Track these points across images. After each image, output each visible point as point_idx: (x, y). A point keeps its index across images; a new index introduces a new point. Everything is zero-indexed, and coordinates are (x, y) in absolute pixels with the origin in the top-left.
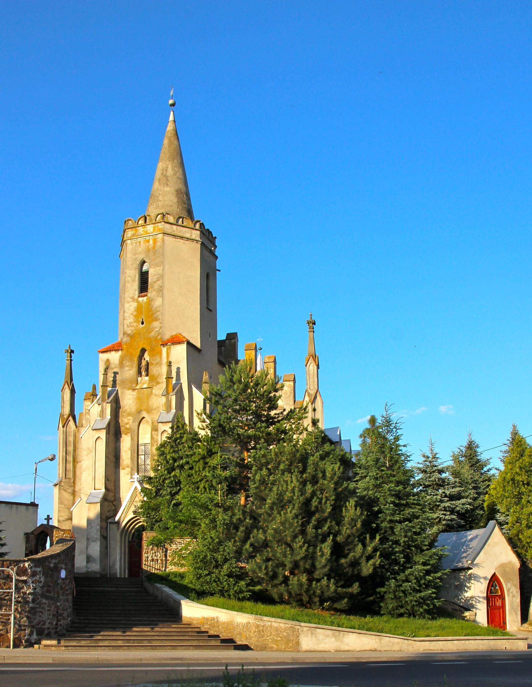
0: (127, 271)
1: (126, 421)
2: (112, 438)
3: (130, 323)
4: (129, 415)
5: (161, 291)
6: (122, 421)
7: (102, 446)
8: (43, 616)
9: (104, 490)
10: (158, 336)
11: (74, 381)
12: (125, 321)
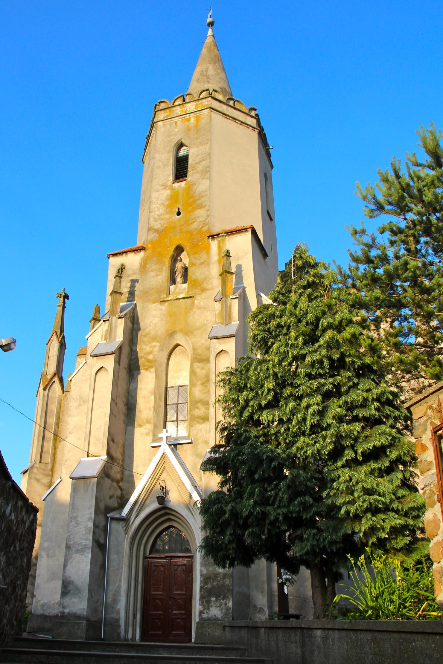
0: (157, 156)
1: (146, 349)
2: (123, 373)
3: (158, 215)
4: (154, 339)
5: (208, 171)
6: (141, 349)
7: (106, 383)
9: (105, 457)
10: (203, 227)
11: (66, 333)
12: (152, 214)
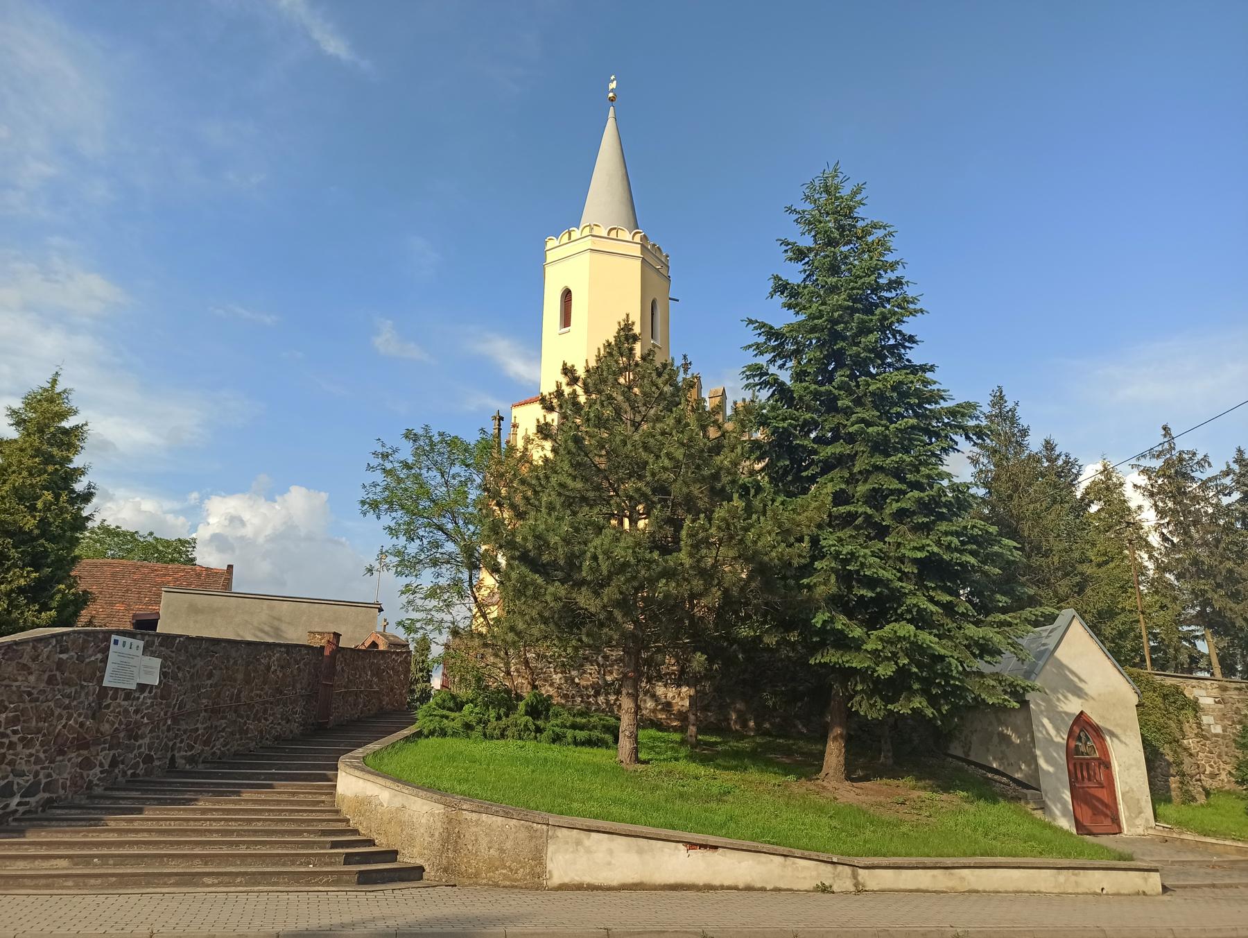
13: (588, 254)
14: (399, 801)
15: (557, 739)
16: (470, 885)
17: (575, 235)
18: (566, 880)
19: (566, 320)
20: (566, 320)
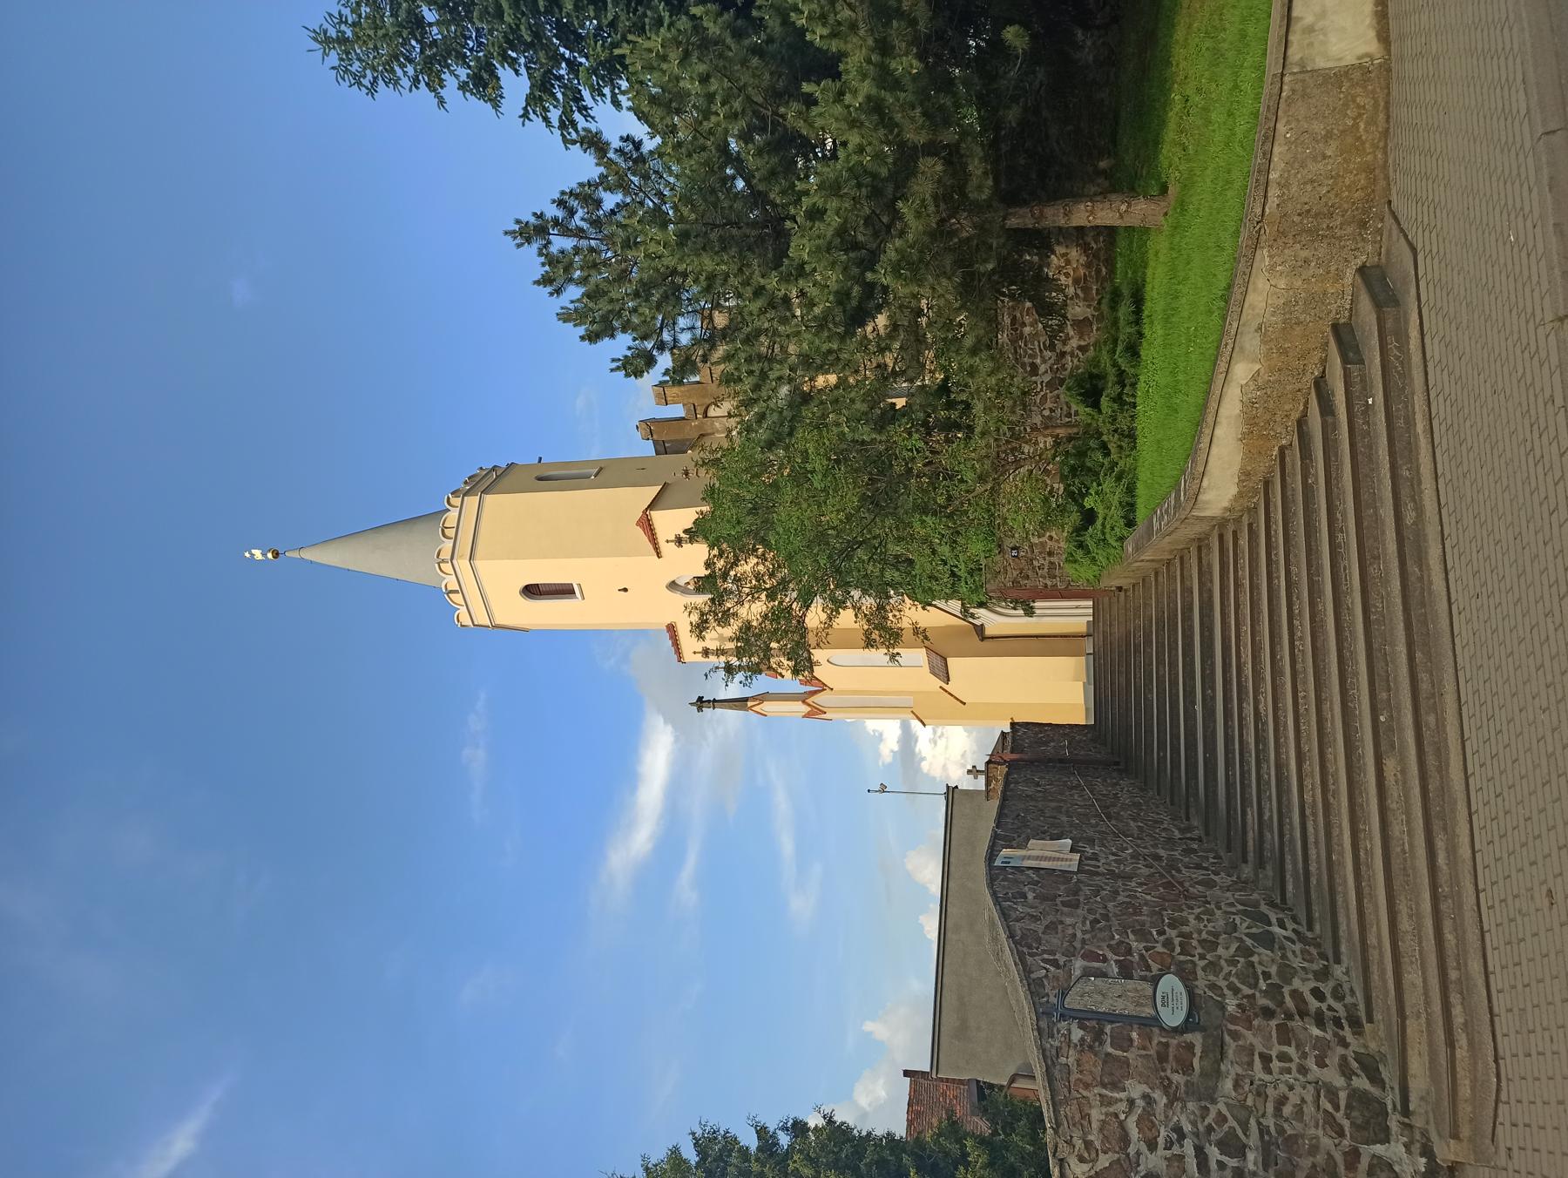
8: (1294, 1099)
13: (478, 563)
14: (1251, 342)
15: (1133, 351)
16: (1387, 178)
17: (454, 586)
18: (1372, 34)
19: (565, 591)
20: (565, 591)
